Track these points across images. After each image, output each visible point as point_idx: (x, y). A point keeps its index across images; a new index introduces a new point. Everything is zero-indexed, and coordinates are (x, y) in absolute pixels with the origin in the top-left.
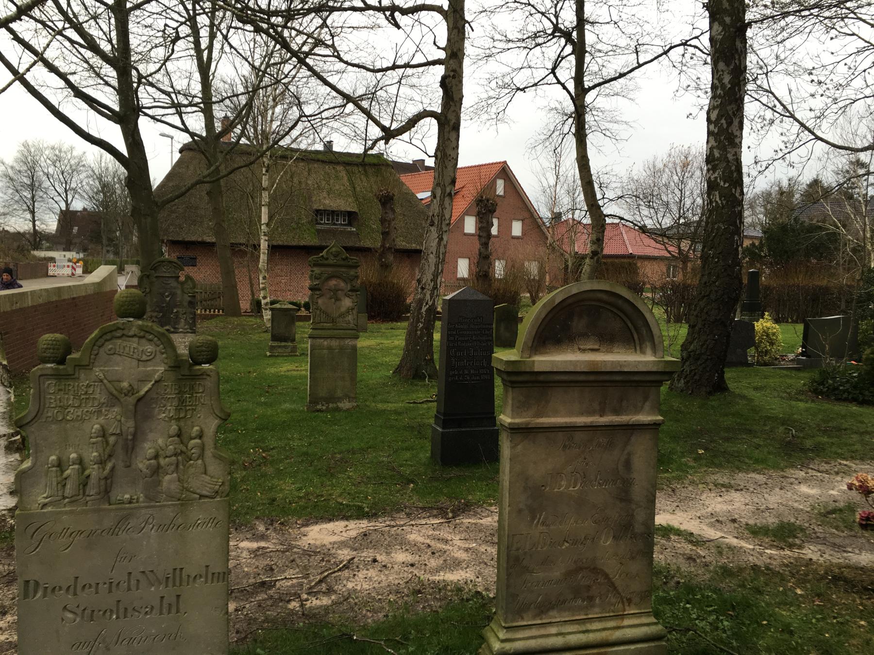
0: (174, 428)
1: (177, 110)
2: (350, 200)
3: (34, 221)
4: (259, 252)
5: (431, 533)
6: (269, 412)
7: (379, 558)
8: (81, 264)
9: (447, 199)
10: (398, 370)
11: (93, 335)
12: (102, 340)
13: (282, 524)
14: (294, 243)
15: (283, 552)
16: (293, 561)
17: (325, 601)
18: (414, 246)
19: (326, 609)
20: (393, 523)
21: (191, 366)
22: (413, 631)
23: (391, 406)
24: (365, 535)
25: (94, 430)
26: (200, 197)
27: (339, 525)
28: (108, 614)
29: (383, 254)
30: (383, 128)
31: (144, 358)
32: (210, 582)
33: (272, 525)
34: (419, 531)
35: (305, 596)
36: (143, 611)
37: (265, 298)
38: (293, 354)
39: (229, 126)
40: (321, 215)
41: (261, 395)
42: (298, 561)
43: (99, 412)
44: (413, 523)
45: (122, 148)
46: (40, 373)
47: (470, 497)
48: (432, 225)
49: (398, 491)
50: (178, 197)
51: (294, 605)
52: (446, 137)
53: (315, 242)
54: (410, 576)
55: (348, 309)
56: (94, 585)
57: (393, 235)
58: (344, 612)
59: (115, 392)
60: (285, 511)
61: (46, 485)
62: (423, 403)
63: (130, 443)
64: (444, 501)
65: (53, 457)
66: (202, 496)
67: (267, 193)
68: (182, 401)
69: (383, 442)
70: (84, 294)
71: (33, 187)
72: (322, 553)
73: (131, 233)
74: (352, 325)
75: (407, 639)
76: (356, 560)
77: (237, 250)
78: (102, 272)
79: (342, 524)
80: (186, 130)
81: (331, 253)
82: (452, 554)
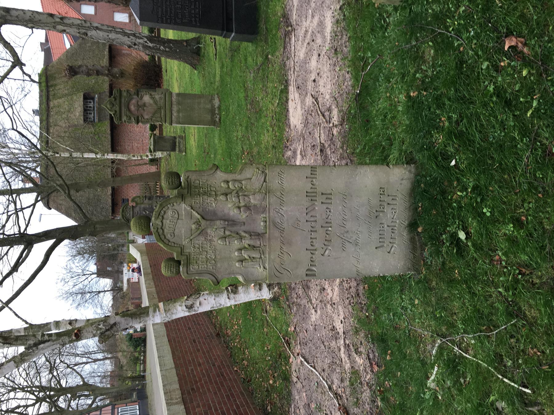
0: (222, 198)
1: (19, 211)
2: (75, 98)
3: (105, 291)
4: (116, 159)
5: (300, 43)
6: (220, 151)
7: (313, 78)
8: (131, 265)
9: (65, 21)
10: (194, 66)
11: (162, 246)
12: (165, 241)
13: (288, 141)
14: (109, 137)
15: (304, 139)
16: (310, 133)
17: (335, 112)
18: (106, 52)
19: (340, 111)
20: (292, 69)
21: (182, 188)
22: (359, 54)
23: (218, 71)
24: (298, 87)
25: (222, 243)
26: (81, 196)
27: (291, 105)
28: (328, 232)
29: (113, 76)
30: (13, 67)
31: (176, 216)
32: (315, 176)
33: (288, 147)
34: (299, 51)
35: (331, 125)
36: (328, 213)
37: (147, 156)
38: (183, 138)
39: (28, 178)
40: (87, 118)
41: (210, 157)
42: (310, 130)
43: (211, 241)
44: (293, 56)
45: (51, 242)
46: (186, 274)
47: (279, 14)
48: (87, 35)
49: (273, 66)
50: (81, 209)
51: (335, 131)
52: (16, 19)
53: (107, 123)
54: (326, 57)
55: (151, 98)
56: (311, 240)
57: (99, 68)
58: (343, 100)
59: (198, 232)
60: (280, 140)
61: (253, 268)
62: (216, 49)
63: (230, 223)
64: (281, 34)
65: (237, 264)
66: (265, 181)
67: (73, 154)
68: (205, 193)
69: (241, 76)
70: (148, 261)
71: (83, 293)
72: (308, 114)
73: (109, 238)
74: (163, 96)
75: (363, 58)
76: (313, 93)
77: (116, 173)
78: (134, 252)
79: (290, 102)
80: (34, 205)
81: (111, 108)
82: (315, 27)
